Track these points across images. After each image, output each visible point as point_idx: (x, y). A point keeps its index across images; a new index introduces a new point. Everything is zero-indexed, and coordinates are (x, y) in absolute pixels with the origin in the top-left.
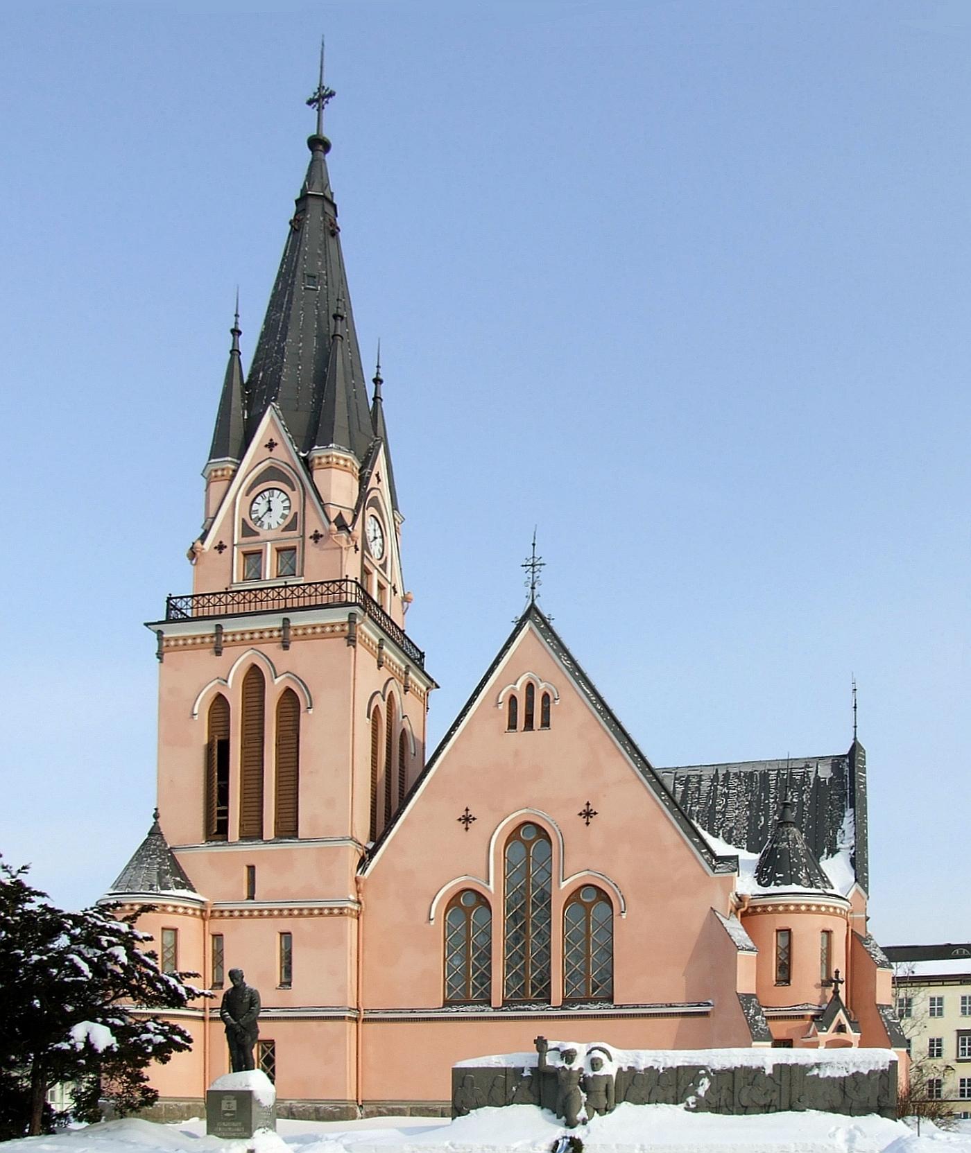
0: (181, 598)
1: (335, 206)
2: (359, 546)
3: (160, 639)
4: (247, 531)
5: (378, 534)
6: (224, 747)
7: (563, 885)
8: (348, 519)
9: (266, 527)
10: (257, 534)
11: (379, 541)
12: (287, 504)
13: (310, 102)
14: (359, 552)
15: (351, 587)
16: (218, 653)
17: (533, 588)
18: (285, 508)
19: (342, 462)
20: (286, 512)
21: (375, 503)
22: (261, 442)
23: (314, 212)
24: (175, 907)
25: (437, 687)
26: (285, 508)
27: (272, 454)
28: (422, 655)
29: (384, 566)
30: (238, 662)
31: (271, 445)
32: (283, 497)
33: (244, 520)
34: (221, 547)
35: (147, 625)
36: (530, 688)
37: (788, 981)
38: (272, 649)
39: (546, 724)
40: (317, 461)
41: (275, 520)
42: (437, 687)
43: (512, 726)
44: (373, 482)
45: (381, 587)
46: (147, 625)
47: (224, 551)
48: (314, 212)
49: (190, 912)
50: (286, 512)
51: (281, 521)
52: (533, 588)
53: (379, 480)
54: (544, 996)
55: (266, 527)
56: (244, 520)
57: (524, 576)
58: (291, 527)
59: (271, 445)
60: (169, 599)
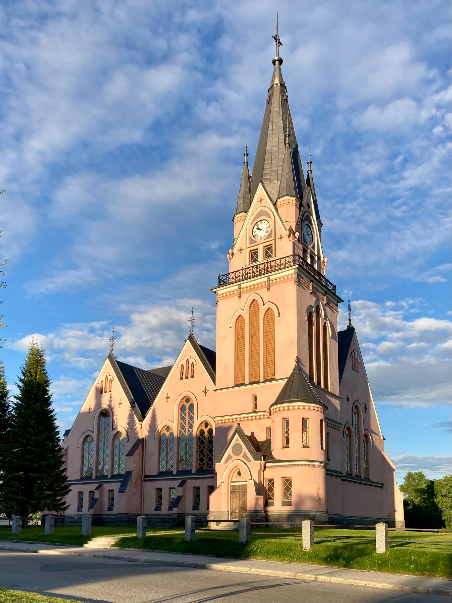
1: (286, 87)
4: (252, 241)
7: (174, 424)
9: (259, 238)
10: (257, 242)
12: (268, 225)
13: (252, 433)
16: (240, 296)
18: (267, 228)
19: (290, 201)
20: (268, 229)
22: (257, 199)
25: (342, 301)
26: (267, 228)
27: (262, 204)
28: (335, 287)
30: (247, 298)
31: (261, 201)
33: (250, 237)
34: (241, 250)
38: (263, 292)
39: (192, 377)
41: (261, 234)
42: (342, 301)
43: (182, 378)
47: (242, 251)
50: (268, 229)
51: (266, 234)
54: (252, 521)
55: (259, 238)
56: (250, 237)
58: (270, 235)
59: (261, 201)
60: (219, 277)
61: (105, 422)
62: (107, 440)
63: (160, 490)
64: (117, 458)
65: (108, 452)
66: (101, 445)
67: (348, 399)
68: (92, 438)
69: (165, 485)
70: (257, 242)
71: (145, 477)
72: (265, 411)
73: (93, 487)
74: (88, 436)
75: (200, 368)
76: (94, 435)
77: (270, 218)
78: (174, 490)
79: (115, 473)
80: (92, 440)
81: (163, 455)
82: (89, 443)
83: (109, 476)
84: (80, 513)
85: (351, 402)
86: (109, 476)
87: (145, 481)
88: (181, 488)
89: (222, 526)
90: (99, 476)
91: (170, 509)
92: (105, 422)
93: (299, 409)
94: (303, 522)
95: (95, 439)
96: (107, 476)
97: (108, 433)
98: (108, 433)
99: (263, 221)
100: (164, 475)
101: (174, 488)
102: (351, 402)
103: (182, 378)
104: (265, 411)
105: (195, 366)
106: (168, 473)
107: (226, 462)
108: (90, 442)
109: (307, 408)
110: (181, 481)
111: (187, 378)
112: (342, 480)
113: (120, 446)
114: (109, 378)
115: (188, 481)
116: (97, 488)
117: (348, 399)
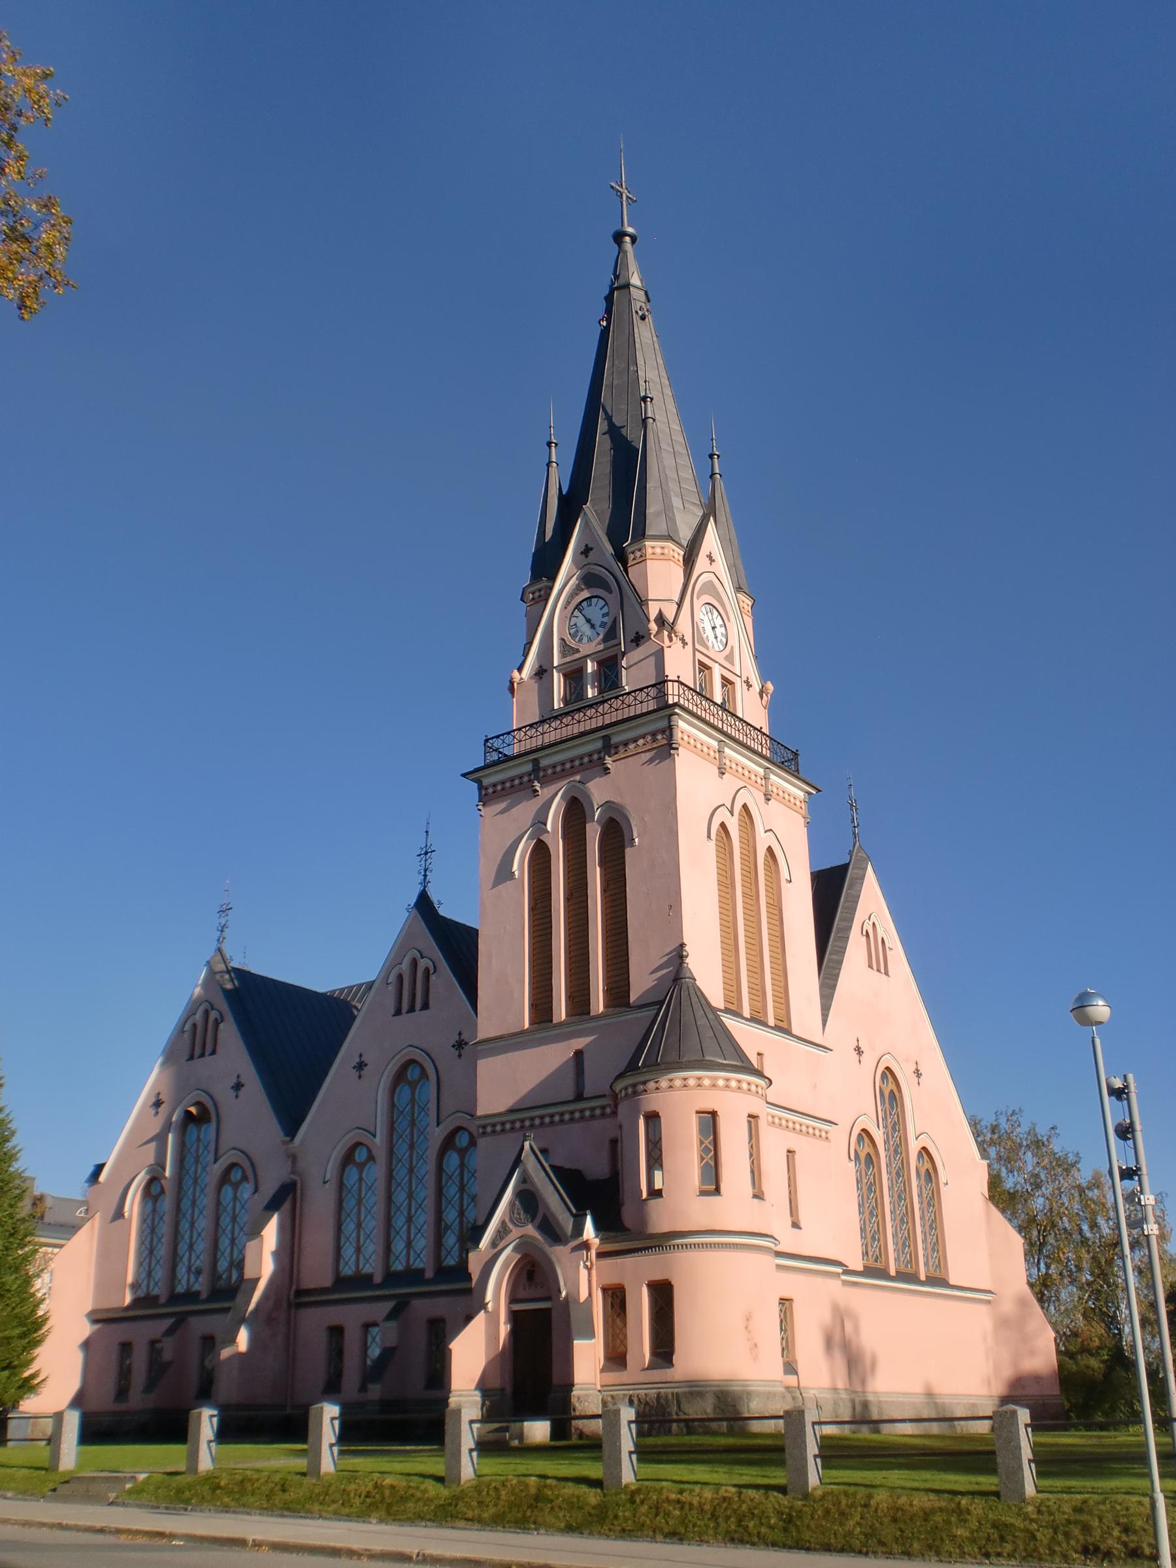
0: (498, 737)
2: (688, 639)
3: (481, 788)
5: (719, 622)
6: (194, 1043)
7: (378, 1140)
8: (669, 616)
10: (578, 651)
11: (720, 631)
12: (605, 610)
14: (689, 647)
15: (676, 700)
17: (425, 876)
18: (604, 615)
20: (605, 619)
21: (709, 588)
23: (824, 1025)
24: (727, 1080)
26: (604, 615)
29: (730, 658)
32: (602, 603)
33: (563, 640)
35: (464, 775)
36: (414, 963)
37: (717, 1191)
39: (426, 1006)
40: (632, 556)
43: (398, 1012)
44: (701, 563)
45: (726, 682)
46: (464, 775)
48: (824, 1025)
49: (745, 1086)
50: (605, 619)
52: (425, 876)
53: (712, 560)
57: (417, 865)
60: (487, 741)
61: (199, 1139)
62: (202, 1190)
63: (336, 1332)
64: (227, 1242)
65: (203, 1223)
66: (186, 1204)
67: (858, 1050)
68: (369, 1151)
69: (351, 1316)
70: (578, 651)
71: (300, 1293)
72: (604, 1096)
73: (158, 1328)
74: (459, 1129)
75: (445, 981)
76: (379, 1142)
77: (610, 592)
78: (377, 1329)
79: (398, 1266)
80: (371, 1158)
81: (349, 1227)
82: (361, 1166)
83: (429, 1274)
84: (123, 1407)
85: (869, 1059)
86: (378, 1279)
87: (300, 1305)
88: (393, 1324)
89: (769, 1426)
90: (398, 1274)
91: (363, 1388)
92: (199, 1139)
93: (714, 1085)
94: (548, 1423)
95: (381, 1154)
96: (422, 1271)
97: (204, 1169)
98: (204, 1169)
99: (594, 600)
100: (349, 1285)
101: (375, 1324)
102: (869, 1059)
103: (191, 1058)
104: (604, 1096)
105: (433, 978)
106: (361, 1281)
107: (779, 1266)
108: (240, 1182)
109: (707, 1082)
110: (173, 1320)
111: (412, 1009)
112: (845, 1283)
113: (360, 1189)
114: (423, 963)
115: (416, 1303)
116: (170, 1332)
117: (858, 1050)
